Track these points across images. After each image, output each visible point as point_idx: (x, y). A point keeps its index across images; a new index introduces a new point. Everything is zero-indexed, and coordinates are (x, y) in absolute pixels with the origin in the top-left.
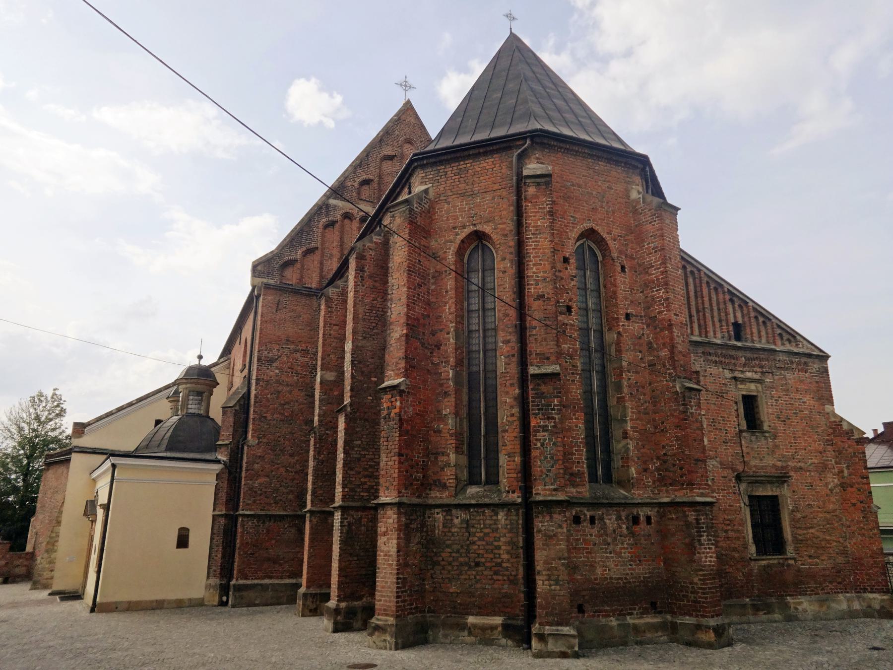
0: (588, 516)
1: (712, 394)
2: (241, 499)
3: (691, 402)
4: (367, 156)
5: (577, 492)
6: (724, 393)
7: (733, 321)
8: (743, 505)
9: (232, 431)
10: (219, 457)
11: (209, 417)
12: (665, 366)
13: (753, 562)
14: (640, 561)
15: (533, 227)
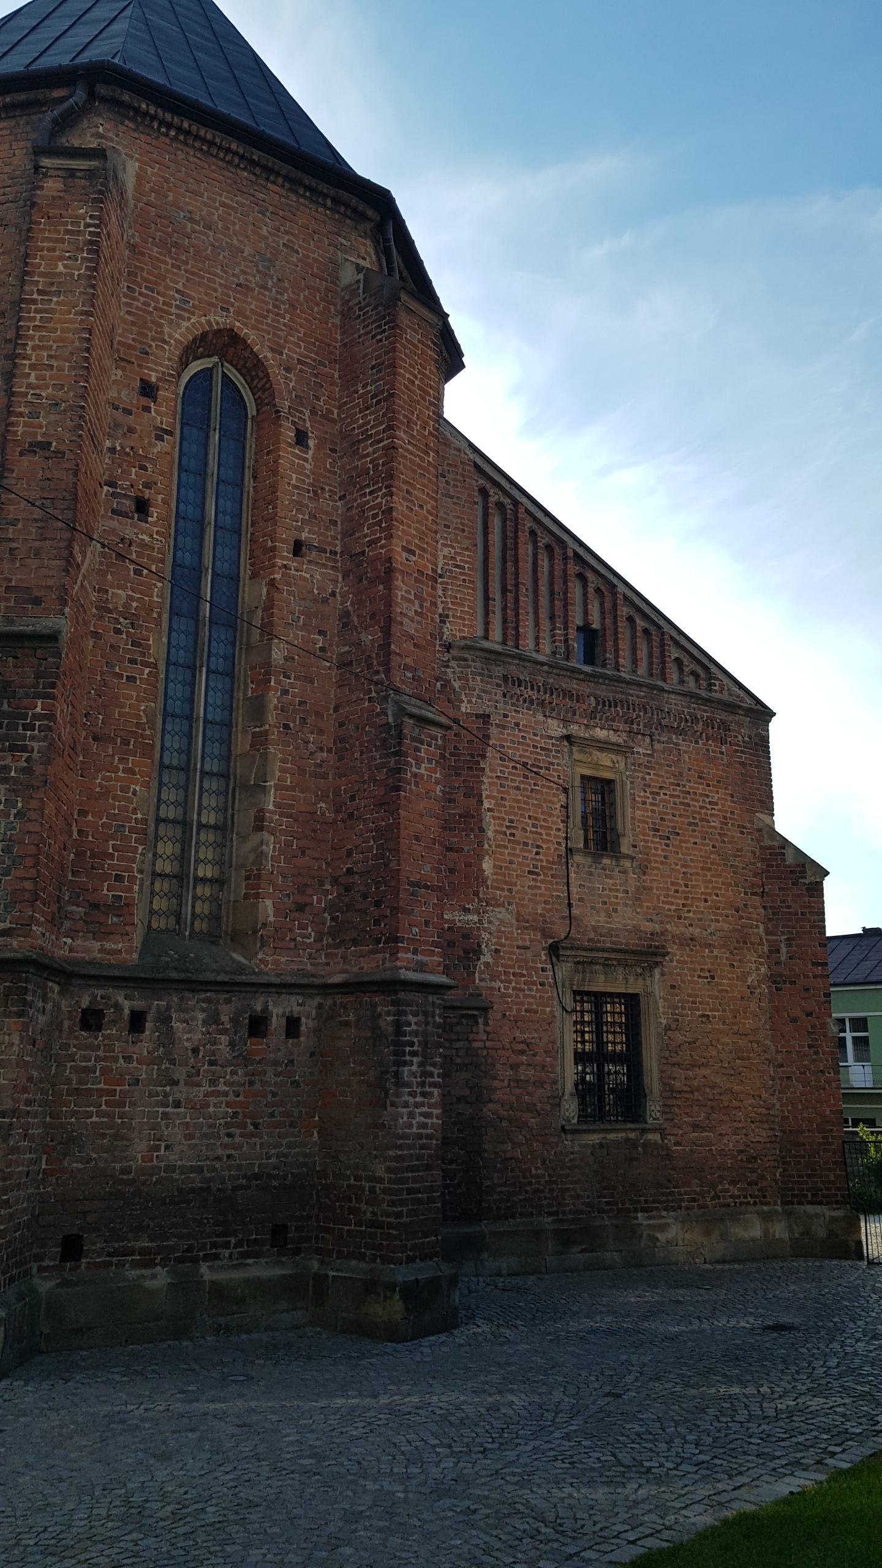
0: (127, 1012)
1: (514, 768)
3: (417, 749)
5: (102, 950)
6: (541, 768)
7: (579, 621)
8: (558, 1012)
12: (370, 666)
13: (569, 1137)
14: (256, 1126)
15: (42, 275)
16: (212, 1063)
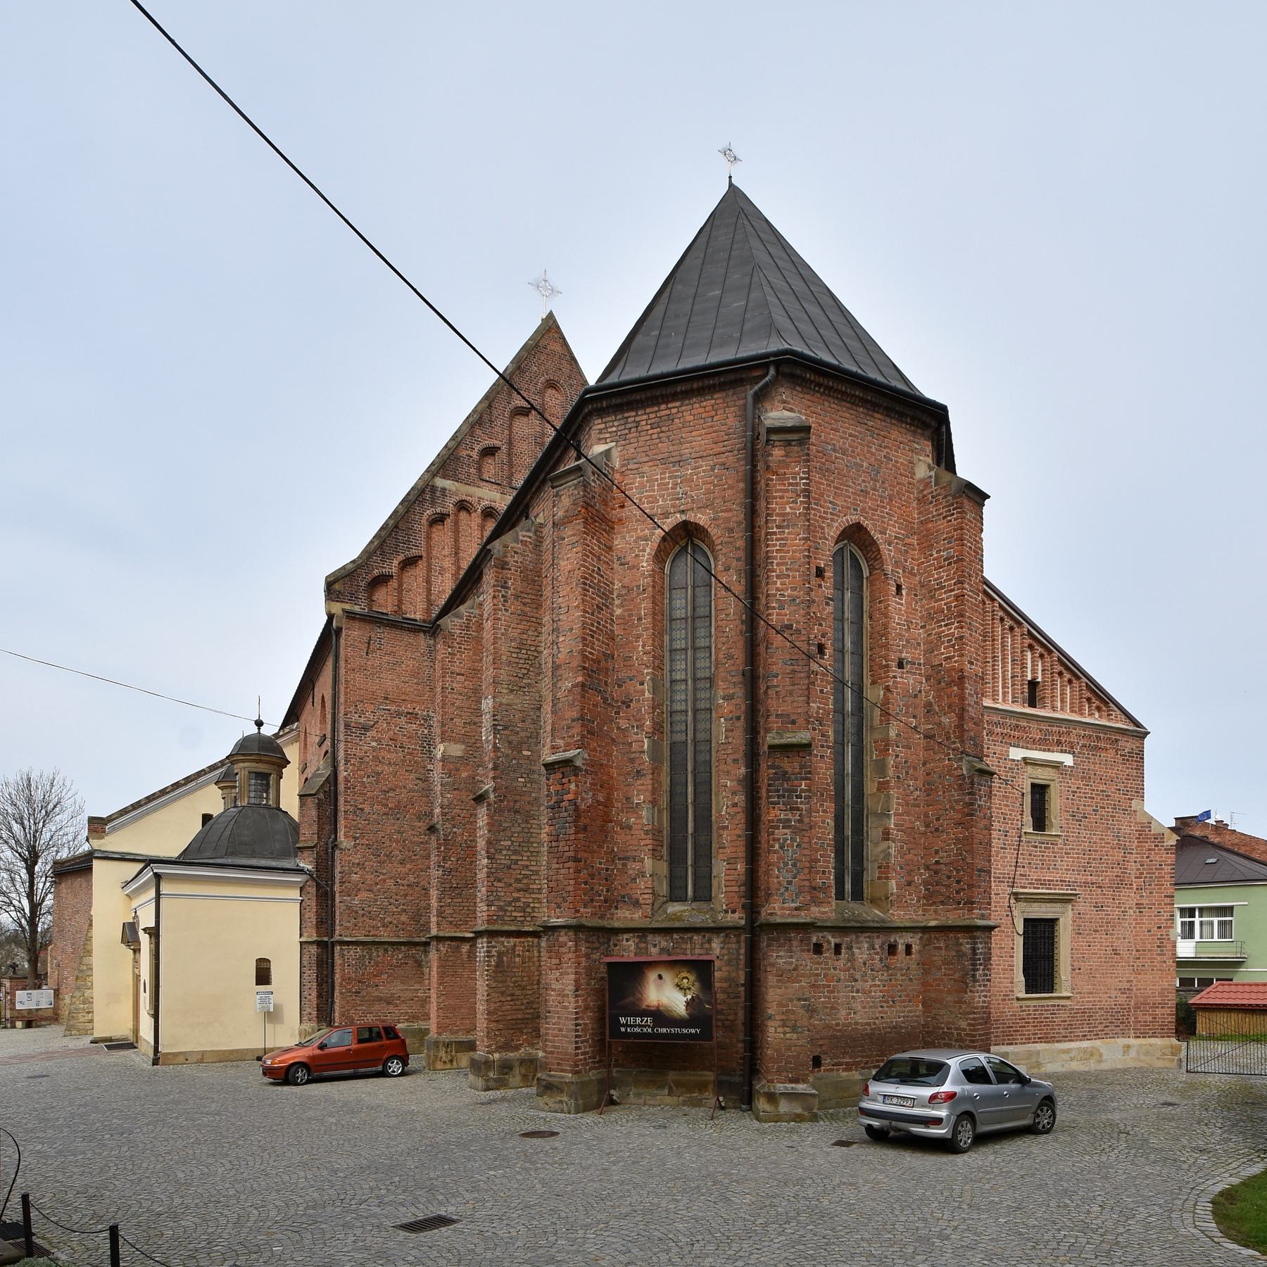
0: (833, 944)
2: (337, 922)
3: (980, 790)
4: (490, 406)
5: (820, 912)
7: (1029, 678)
9: (316, 828)
10: (302, 865)
11: (281, 810)
12: (948, 738)
14: (893, 1002)
15: (778, 515)
16: (872, 970)
